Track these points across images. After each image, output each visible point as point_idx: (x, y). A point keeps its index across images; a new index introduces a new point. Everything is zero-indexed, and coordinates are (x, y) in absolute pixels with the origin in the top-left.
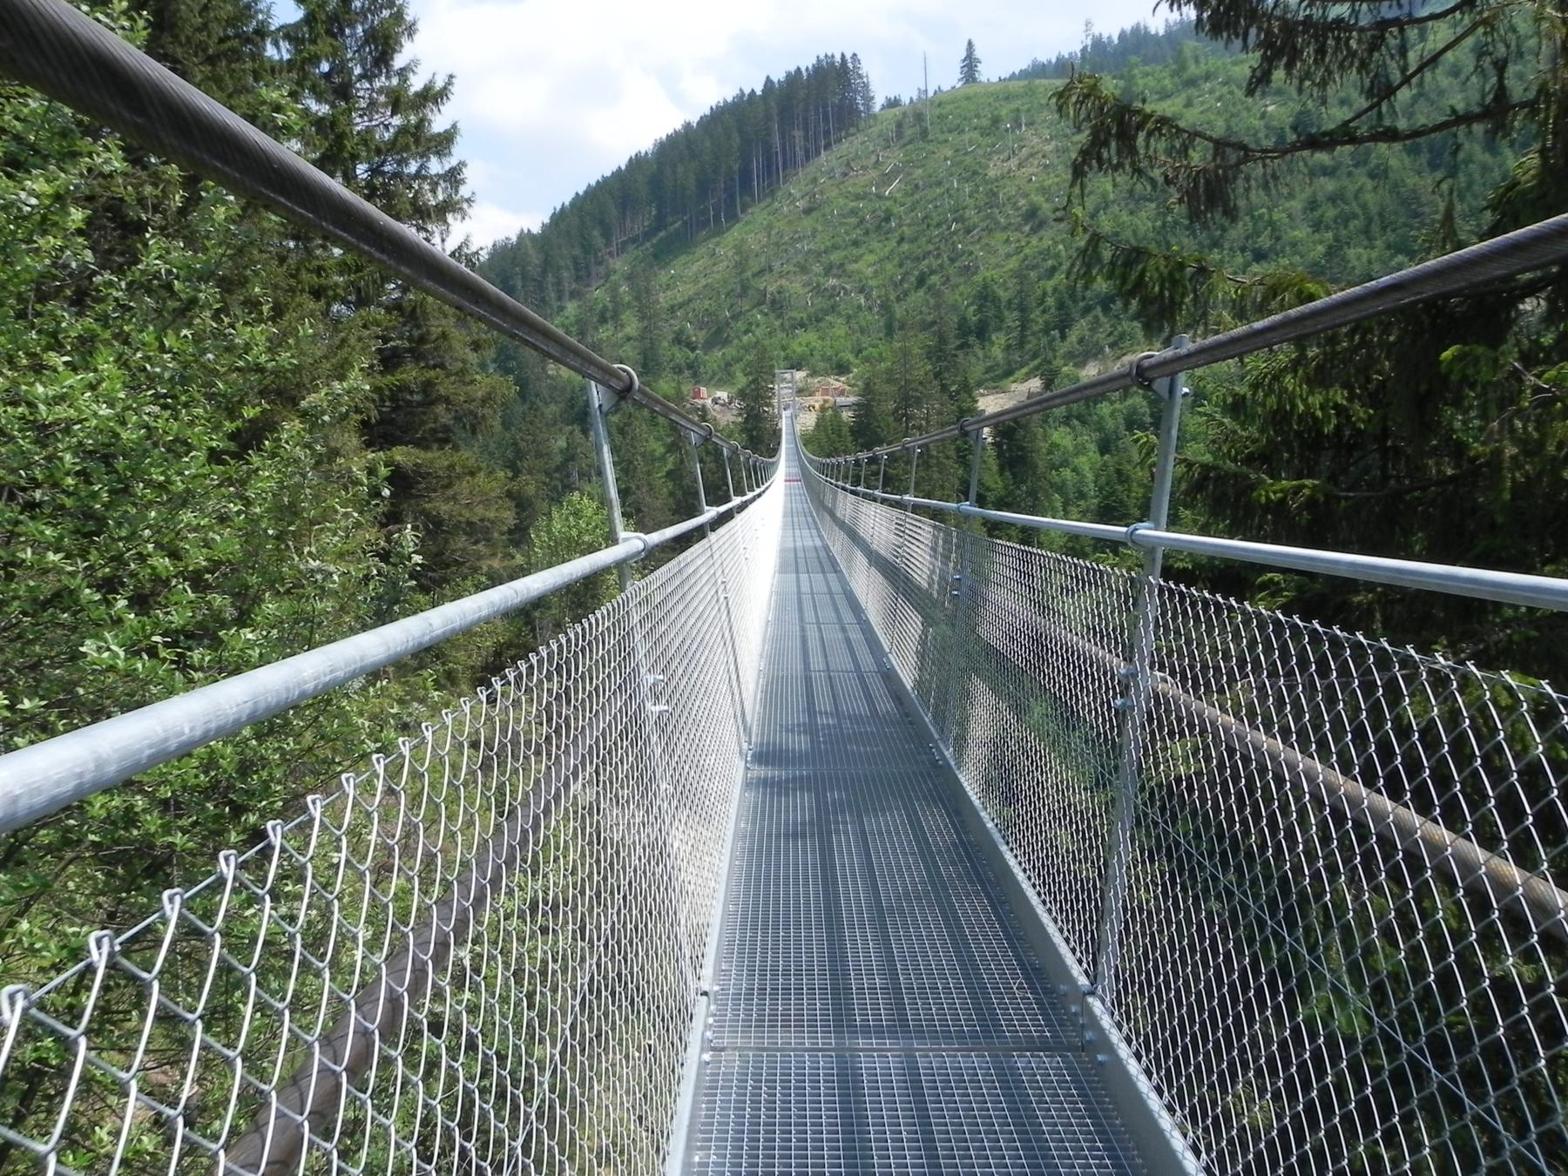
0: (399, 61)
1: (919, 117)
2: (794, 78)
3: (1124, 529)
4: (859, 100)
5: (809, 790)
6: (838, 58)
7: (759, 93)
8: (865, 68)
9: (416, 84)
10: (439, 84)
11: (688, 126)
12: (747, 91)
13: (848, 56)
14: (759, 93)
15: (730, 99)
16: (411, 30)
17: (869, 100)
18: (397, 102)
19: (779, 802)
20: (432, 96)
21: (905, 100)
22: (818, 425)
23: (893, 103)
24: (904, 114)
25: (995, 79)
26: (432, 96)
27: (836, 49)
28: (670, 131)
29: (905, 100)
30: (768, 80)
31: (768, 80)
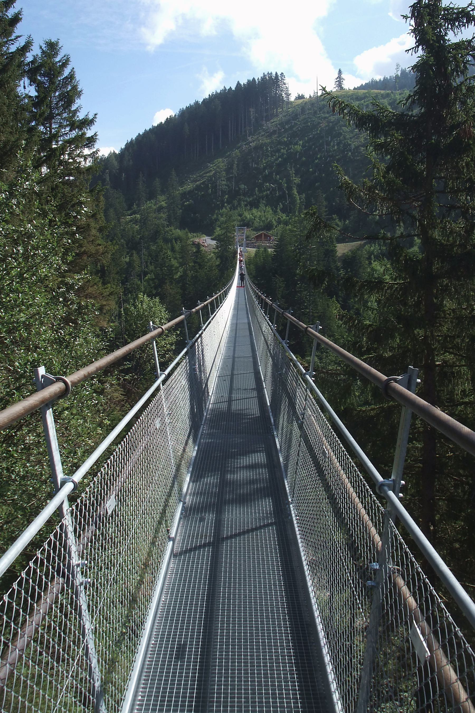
0: (74, 108)
1: (313, 104)
2: (251, 83)
3: (385, 378)
4: (284, 95)
5: (232, 413)
6: (274, 74)
7: (233, 89)
8: (287, 80)
9: (81, 116)
10: (91, 117)
11: (197, 103)
12: (228, 88)
13: (279, 74)
14: (233, 89)
15: (219, 91)
16: (79, 94)
17: (288, 95)
18: (73, 126)
19: (244, 511)
20: (87, 122)
21: (307, 96)
22: (256, 255)
23: (300, 97)
24: (306, 103)
25: (352, 88)
26: (87, 122)
27: (274, 69)
28: (188, 105)
29: (307, 96)
30: (238, 83)
31: (238, 83)
